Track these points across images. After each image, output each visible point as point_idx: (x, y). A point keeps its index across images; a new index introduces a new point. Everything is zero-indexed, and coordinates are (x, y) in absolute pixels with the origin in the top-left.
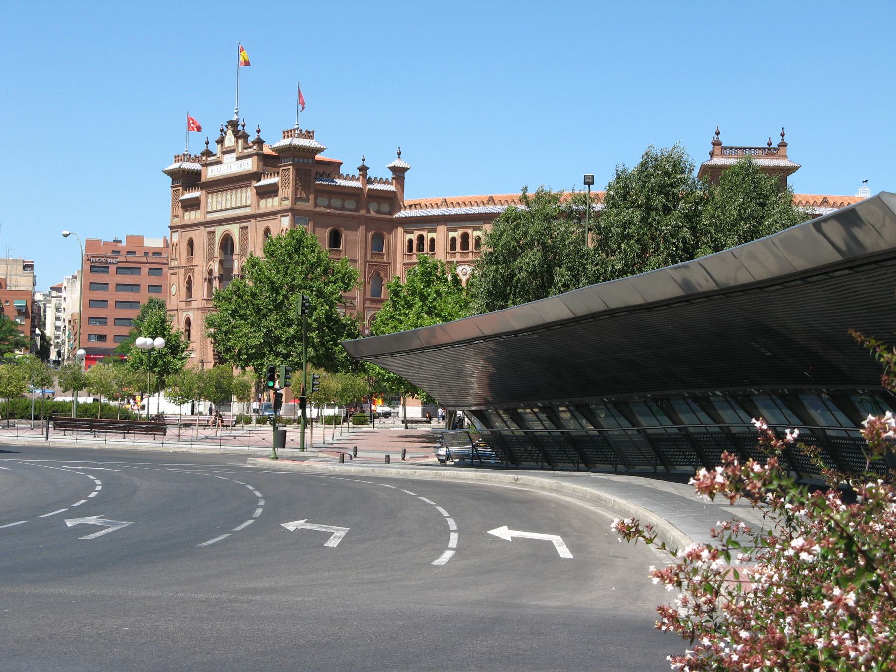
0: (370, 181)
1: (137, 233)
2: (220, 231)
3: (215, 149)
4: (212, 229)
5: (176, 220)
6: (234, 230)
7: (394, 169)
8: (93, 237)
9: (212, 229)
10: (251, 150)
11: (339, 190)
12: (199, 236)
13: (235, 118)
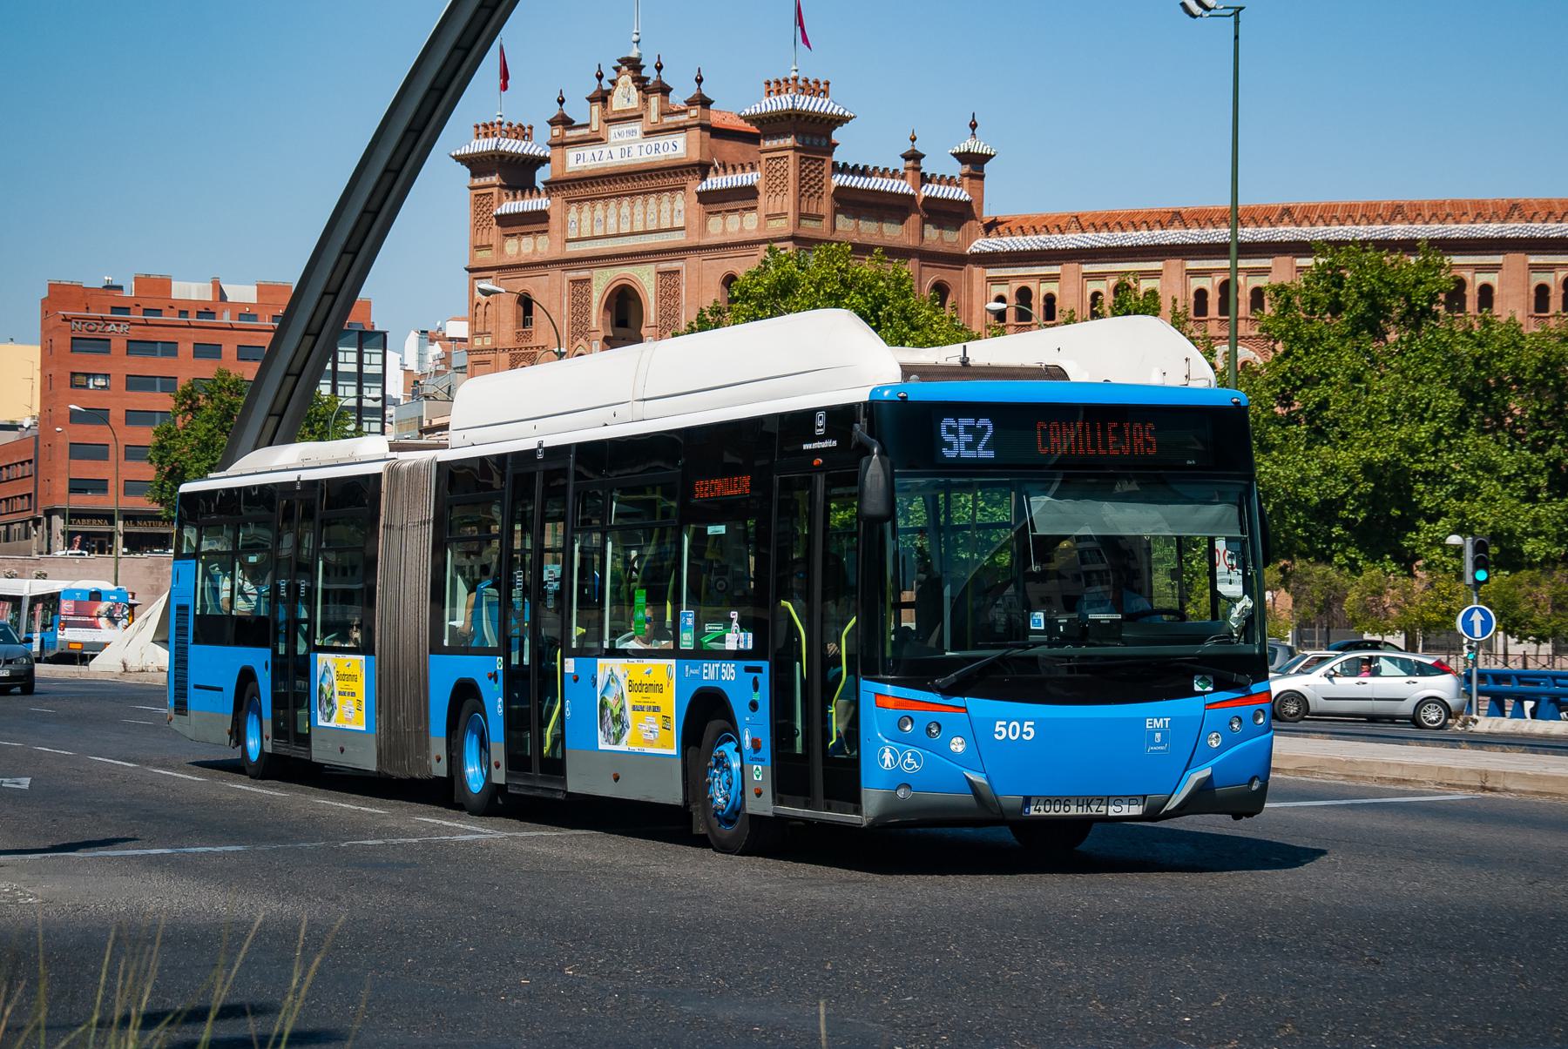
0: (925, 179)
1: (156, 271)
2: (602, 281)
3: (579, 110)
4: (583, 274)
5: (482, 254)
6: (645, 279)
7: (963, 157)
8: (66, 278)
9: (583, 274)
10: (684, 117)
11: (872, 200)
12: (550, 291)
13: (634, 54)
